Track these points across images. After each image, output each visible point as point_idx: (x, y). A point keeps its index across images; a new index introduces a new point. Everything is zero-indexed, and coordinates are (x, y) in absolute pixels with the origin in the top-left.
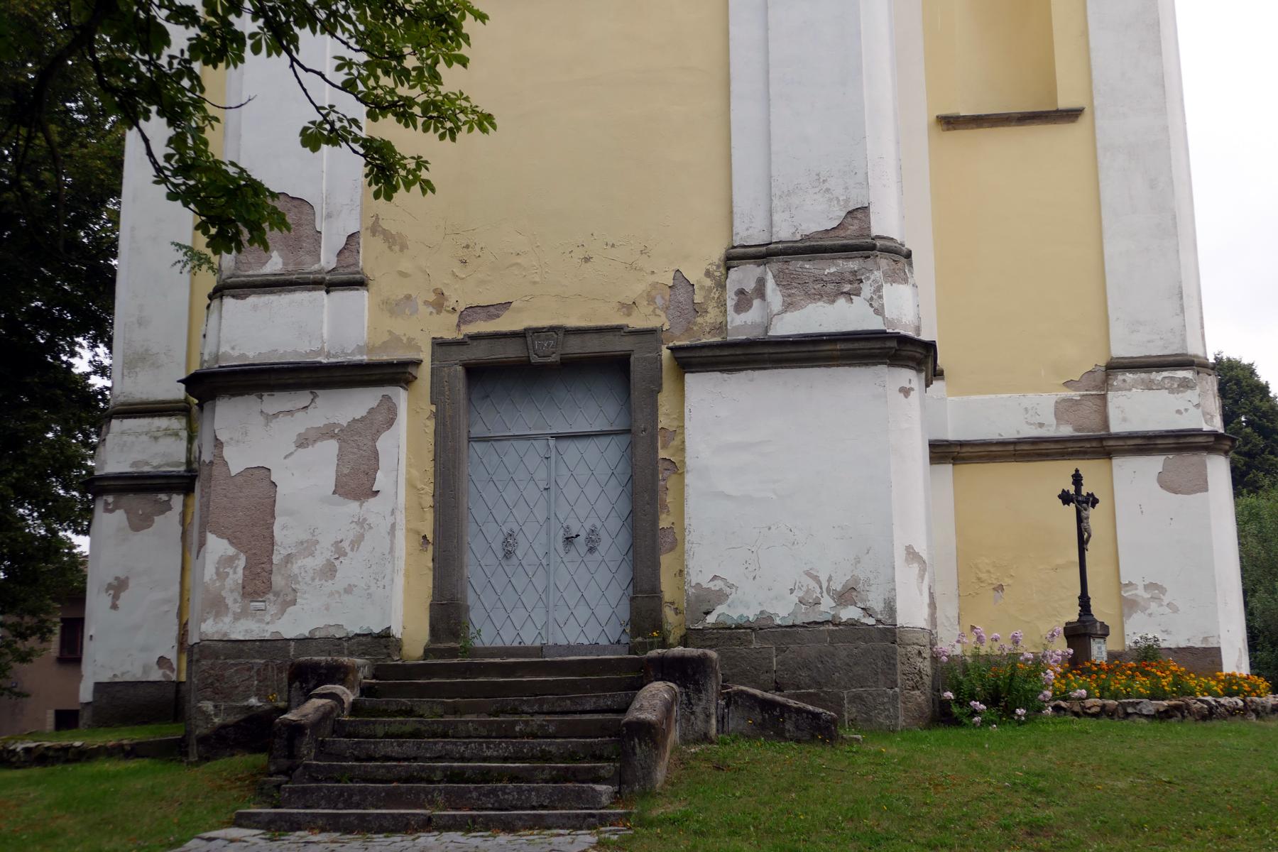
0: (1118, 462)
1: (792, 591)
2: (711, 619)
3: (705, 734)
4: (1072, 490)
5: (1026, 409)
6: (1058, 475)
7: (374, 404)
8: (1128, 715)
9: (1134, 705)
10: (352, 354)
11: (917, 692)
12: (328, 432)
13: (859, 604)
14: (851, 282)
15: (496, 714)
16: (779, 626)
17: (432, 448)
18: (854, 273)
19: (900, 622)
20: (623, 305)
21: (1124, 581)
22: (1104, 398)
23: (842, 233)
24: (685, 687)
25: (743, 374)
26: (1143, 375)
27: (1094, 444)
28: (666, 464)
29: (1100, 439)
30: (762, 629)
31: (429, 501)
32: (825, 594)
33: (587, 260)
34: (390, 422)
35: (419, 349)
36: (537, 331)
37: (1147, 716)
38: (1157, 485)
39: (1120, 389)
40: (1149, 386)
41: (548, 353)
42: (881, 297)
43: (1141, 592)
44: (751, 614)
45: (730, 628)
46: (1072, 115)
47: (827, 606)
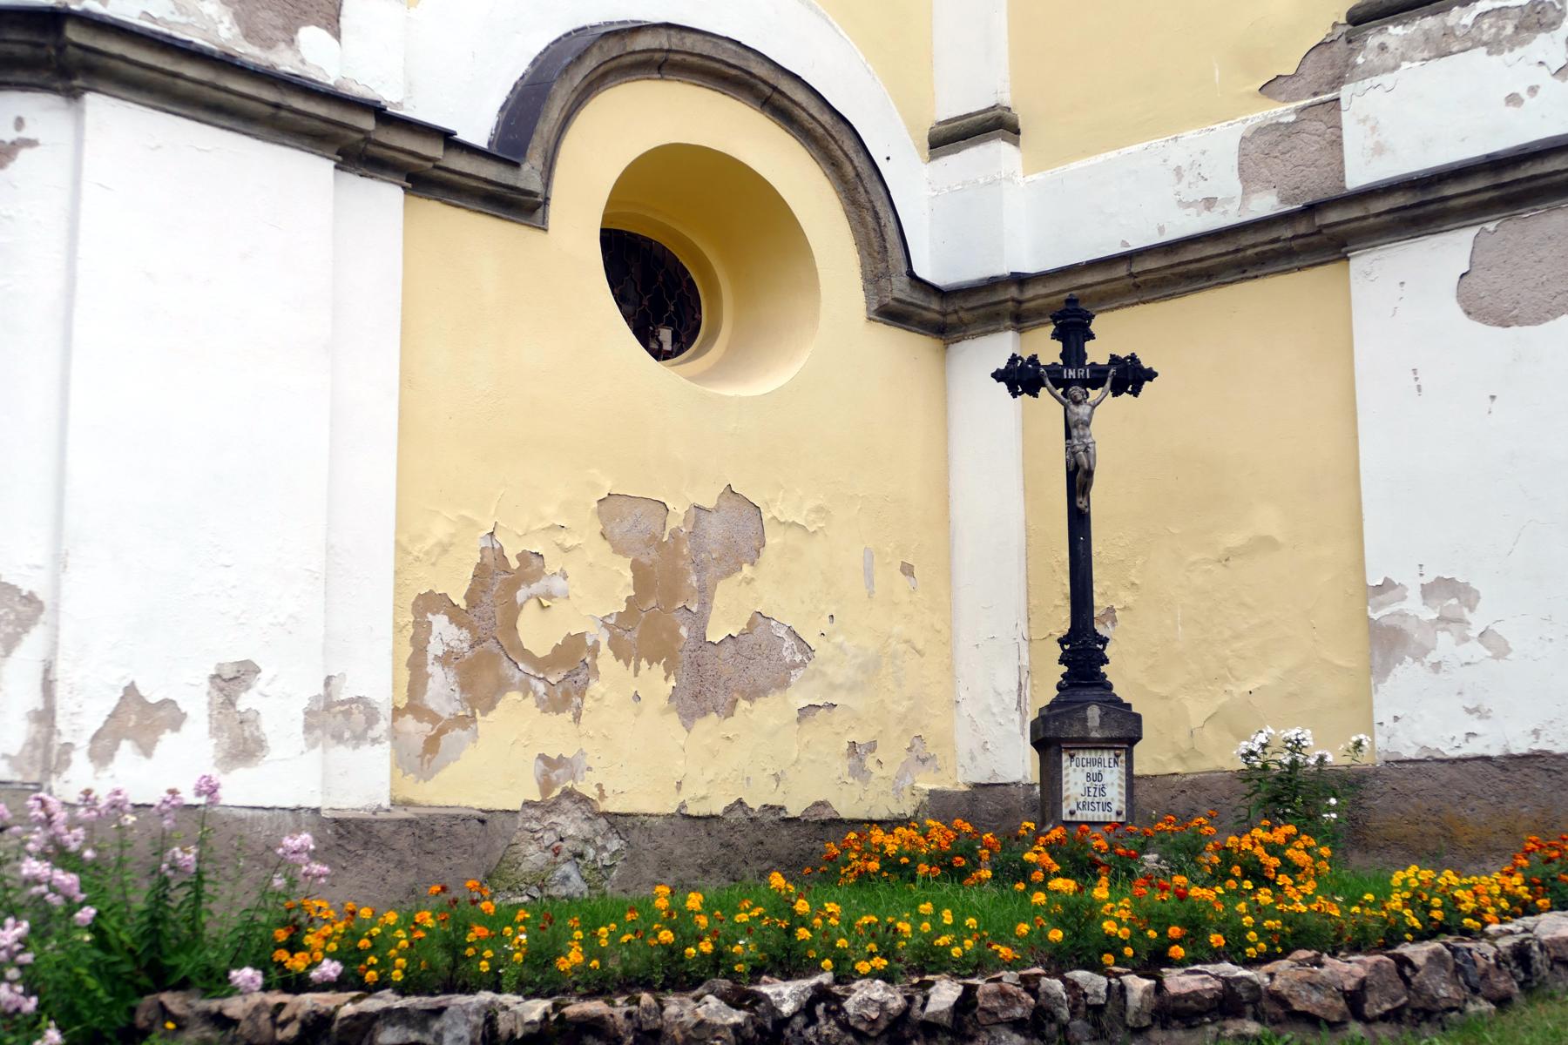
5: (1178, 171)
21: (1375, 580)
27: (1302, 228)
38: (1457, 311)
39: (1372, 72)
43: (1414, 606)
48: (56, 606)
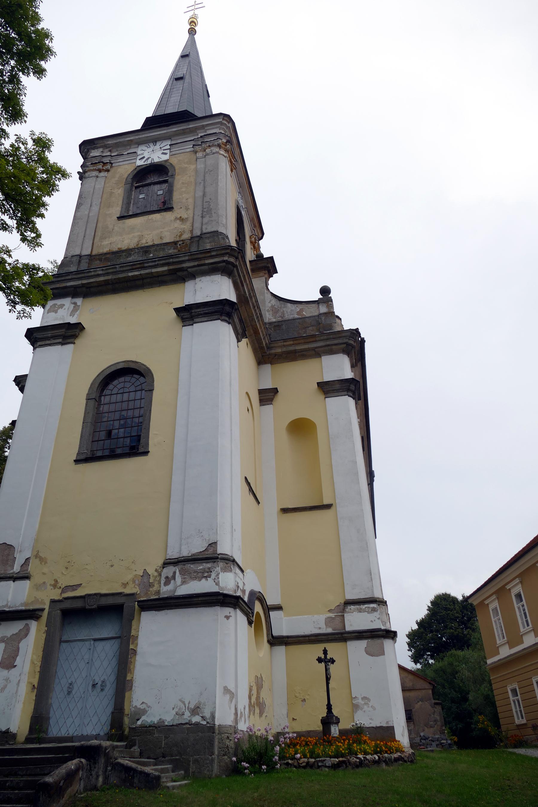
1: (173, 709)
2: (139, 723)
3: (95, 786)
6: (317, 650)
7: (21, 627)
8: (319, 767)
9: (322, 761)
10: (19, 606)
11: (226, 757)
13: (200, 715)
14: (208, 572)
15: (7, 776)
16: (167, 726)
17: (43, 646)
18: (209, 568)
19: (217, 723)
20: (123, 584)
21: (354, 696)
23: (206, 553)
24: (90, 761)
25: (163, 611)
26: (358, 606)
27: (339, 636)
28: (132, 651)
29: (342, 634)
30: (159, 727)
31: (38, 669)
32: (187, 710)
33: (112, 566)
34: (26, 635)
35: (45, 604)
36: (89, 595)
37: (328, 767)
39: (349, 613)
40: (360, 611)
41: (93, 605)
42: (218, 578)
44: (155, 720)
45: (146, 727)
46: (328, 507)
48: (237, 695)
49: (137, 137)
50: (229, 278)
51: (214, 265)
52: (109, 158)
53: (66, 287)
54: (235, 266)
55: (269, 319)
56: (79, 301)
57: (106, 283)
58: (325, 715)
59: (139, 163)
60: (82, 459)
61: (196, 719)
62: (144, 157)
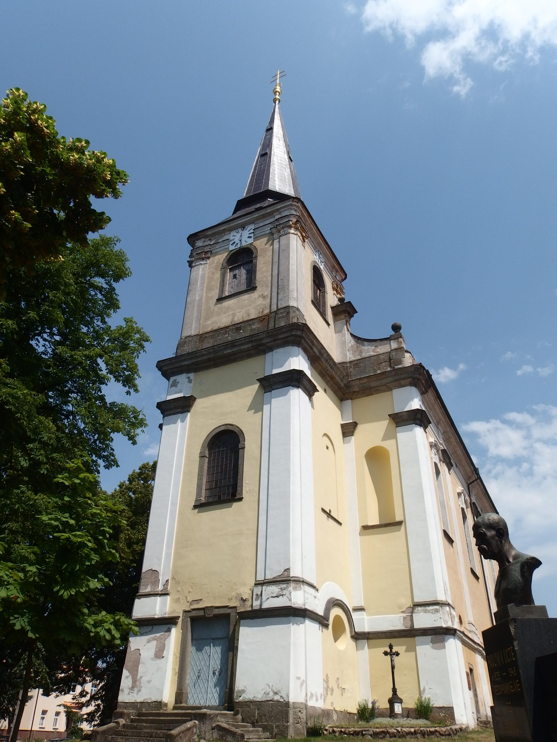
0: (417, 638)
2: (241, 699)
4: (389, 650)
12: (154, 639)
22: (412, 616)
26: (424, 608)
40: (426, 611)
47: (271, 696)
49: (228, 226)
50: (299, 347)
51: (286, 339)
52: (209, 247)
53: (182, 366)
54: (301, 337)
55: (350, 358)
56: (192, 375)
57: (209, 360)
58: (391, 696)
59: (232, 248)
60: (199, 506)
61: (277, 698)
62: (235, 242)
